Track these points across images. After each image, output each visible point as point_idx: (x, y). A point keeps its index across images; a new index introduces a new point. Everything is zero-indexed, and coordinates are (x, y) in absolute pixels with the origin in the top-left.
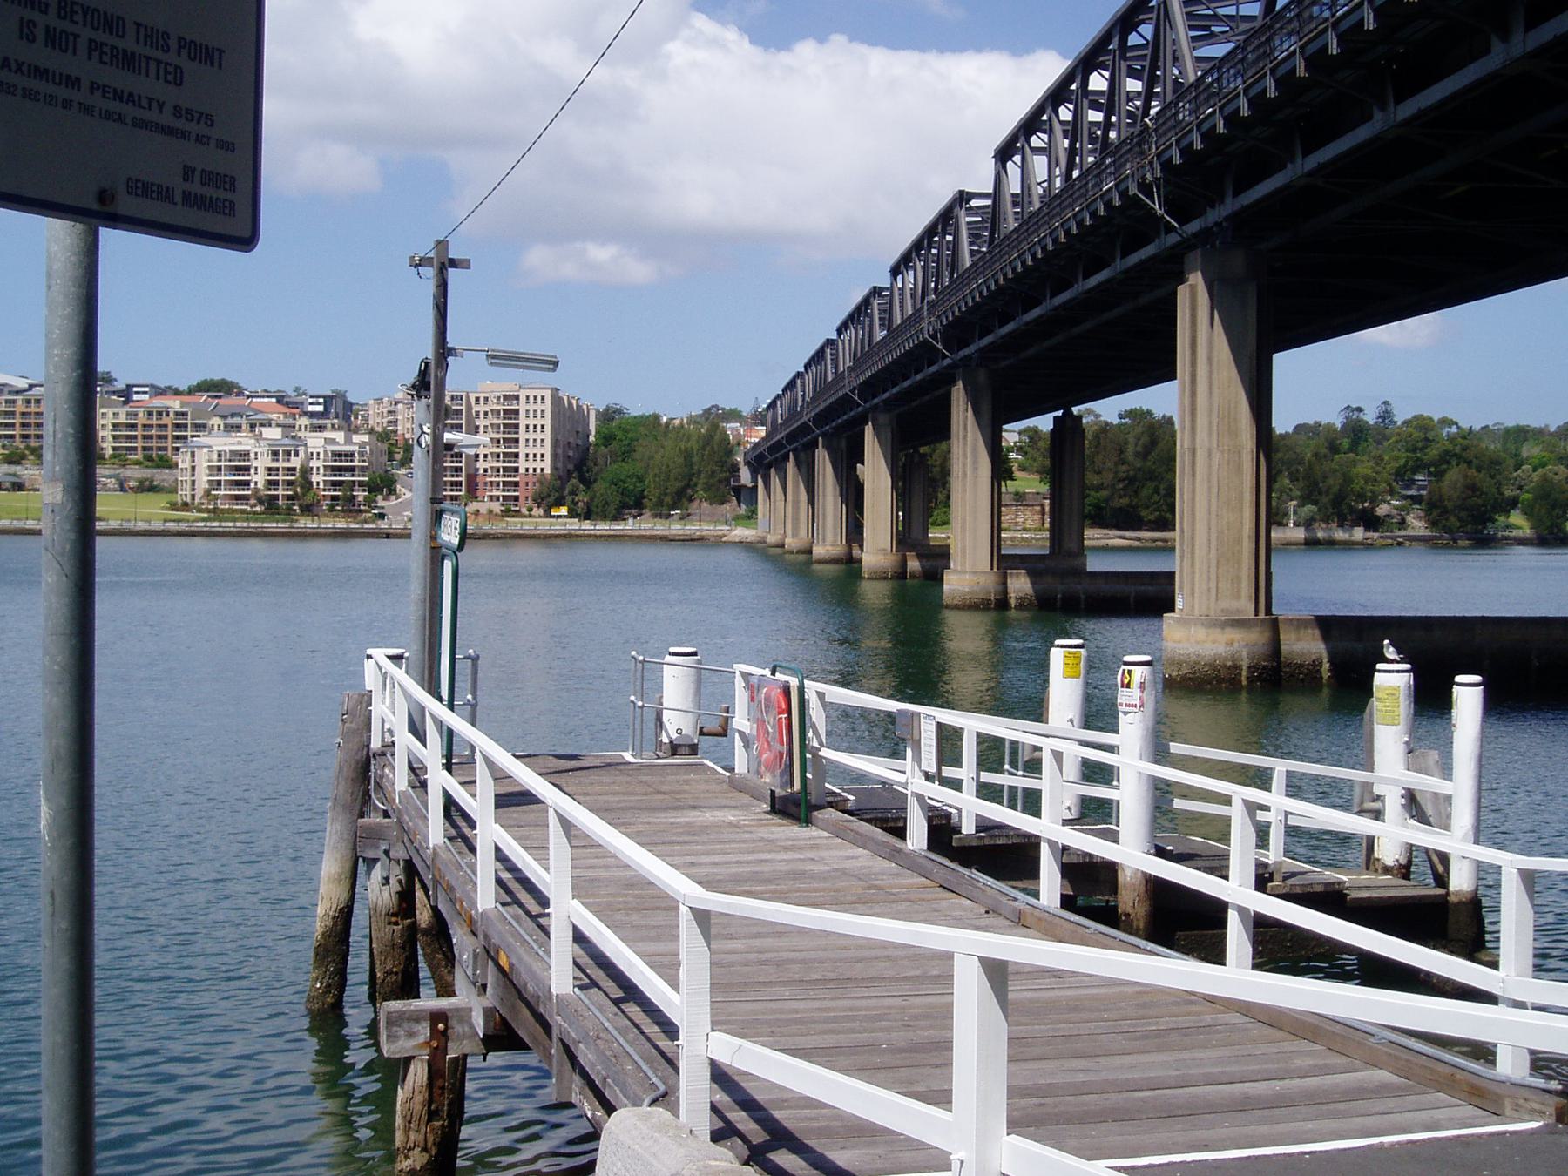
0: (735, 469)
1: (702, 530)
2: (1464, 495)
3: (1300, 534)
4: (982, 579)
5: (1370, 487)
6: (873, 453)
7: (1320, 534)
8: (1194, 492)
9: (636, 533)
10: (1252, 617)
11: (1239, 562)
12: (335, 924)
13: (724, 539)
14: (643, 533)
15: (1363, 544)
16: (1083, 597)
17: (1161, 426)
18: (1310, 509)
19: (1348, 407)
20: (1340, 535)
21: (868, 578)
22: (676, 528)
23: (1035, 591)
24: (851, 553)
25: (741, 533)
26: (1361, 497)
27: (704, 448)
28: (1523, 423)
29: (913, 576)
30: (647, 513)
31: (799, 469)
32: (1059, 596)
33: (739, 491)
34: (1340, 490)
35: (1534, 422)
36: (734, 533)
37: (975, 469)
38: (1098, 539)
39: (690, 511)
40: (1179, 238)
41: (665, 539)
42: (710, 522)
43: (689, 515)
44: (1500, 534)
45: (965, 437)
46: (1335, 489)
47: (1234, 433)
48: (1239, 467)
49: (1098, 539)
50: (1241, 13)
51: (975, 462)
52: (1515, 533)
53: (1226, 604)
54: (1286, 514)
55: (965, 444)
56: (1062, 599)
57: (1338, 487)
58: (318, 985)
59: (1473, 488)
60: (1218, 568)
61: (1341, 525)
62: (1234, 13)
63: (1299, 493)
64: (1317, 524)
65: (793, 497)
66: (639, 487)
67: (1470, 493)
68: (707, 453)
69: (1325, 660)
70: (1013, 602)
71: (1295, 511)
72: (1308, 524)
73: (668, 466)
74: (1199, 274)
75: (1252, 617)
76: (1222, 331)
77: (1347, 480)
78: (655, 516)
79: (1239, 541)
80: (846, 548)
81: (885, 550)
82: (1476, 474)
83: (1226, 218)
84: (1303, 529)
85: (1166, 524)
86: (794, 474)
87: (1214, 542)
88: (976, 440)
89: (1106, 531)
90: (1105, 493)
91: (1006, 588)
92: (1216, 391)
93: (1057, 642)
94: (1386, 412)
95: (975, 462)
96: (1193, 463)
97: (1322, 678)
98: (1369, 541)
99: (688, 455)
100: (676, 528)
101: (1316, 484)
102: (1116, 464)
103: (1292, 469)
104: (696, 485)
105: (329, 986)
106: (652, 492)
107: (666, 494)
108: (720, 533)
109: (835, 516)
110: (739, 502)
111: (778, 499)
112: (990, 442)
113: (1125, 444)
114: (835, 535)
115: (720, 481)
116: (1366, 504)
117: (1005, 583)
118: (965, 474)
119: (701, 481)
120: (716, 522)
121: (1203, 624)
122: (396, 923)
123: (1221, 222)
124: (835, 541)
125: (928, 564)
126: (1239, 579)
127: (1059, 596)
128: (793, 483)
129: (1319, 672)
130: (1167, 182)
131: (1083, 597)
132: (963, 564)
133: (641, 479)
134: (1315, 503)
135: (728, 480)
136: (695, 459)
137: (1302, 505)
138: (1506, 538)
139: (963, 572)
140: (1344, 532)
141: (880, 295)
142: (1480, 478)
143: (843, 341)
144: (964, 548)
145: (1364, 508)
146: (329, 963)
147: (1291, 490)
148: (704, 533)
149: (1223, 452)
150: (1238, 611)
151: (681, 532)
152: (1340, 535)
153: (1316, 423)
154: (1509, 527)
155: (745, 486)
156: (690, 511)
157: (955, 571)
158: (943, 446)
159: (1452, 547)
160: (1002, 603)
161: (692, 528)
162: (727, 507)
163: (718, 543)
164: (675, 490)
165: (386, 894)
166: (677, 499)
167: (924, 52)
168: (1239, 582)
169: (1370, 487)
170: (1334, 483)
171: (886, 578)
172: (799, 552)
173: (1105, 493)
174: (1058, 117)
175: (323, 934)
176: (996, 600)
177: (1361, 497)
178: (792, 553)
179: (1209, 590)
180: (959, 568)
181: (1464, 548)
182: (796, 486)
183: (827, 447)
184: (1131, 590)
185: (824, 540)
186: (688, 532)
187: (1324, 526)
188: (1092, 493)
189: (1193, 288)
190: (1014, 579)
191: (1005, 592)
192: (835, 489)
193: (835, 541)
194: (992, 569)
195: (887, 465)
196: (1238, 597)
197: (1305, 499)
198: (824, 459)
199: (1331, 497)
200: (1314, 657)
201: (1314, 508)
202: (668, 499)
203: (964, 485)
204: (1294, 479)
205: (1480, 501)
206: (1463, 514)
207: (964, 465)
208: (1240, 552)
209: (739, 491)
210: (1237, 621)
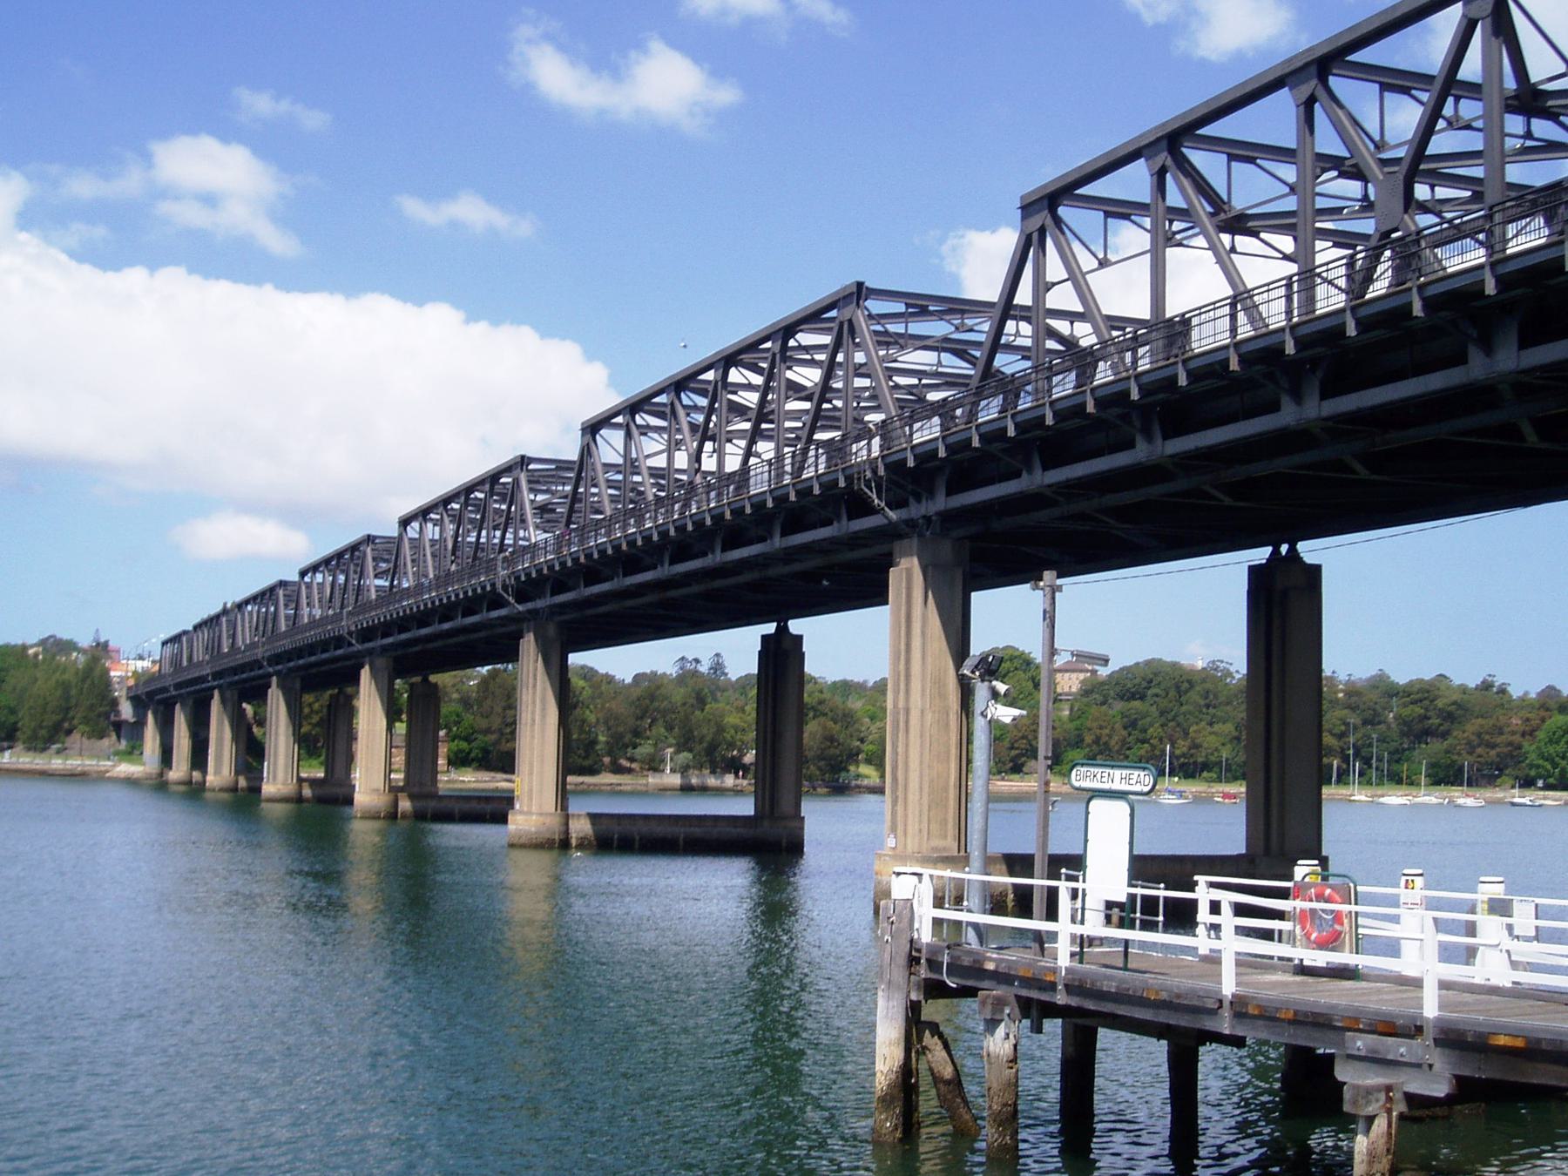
0: (114, 703)
1: (84, 765)
2: (823, 746)
3: (676, 780)
4: (548, 820)
5: (739, 736)
6: (370, 696)
7: (694, 781)
8: (907, 745)
9: (14, 767)
10: (956, 854)
11: (946, 807)
12: (897, 1077)
13: (108, 775)
14: (20, 766)
15: (734, 791)
16: (637, 838)
17: (176, 661)
18: (685, 756)
19: (683, 658)
20: (712, 781)
21: (361, 818)
22: (57, 763)
23: (594, 831)
24: (301, 793)
25: (125, 769)
26: (731, 746)
27: (84, 680)
28: (849, 678)
29: (404, 816)
30: (20, 747)
31: (225, 708)
32: (616, 836)
33: (118, 726)
34: (713, 739)
35: (856, 676)
36: (118, 769)
37: (544, 716)
38: (485, 781)
39: (66, 745)
40: (886, 521)
41: (44, 774)
42: (92, 757)
43: (66, 749)
44: (853, 783)
45: (535, 686)
46: (708, 738)
47: (943, 696)
48: (947, 725)
49: (485, 781)
50: (909, 332)
51: (544, 709)
52: (866, 782)
53: (937, 843)
54: (663, 761)
55: (534, 693)
56: (618, 838)
57: (711, 736)
58: (888, 1124)
59: (831, 739)
60: (929, 811)
61: (713, 772)
62: (903, 331)
63: (674, 742)
64: (691, 771)
65: (217, 733)
66: (12, 719)
67: (829, 744)
68: (86, 686)
69: (1010, 892)
70: (574, 842)
71: (671, 759)
72: (684, 770)
73: (45, 699)
74: (915, 560)
75: (956, 854)
76: (934, 605)
77: (721, 729)
78: (29, 749)
79: (946, 789)
80: (296, 787)
81: (378, 790)
82: (833, 726)
83: (938, 514)
84: (679, 775)
85: (513, 772)
86: (219, 712)
87: (926, 789)
88: (544, 689)
89: (492, 774)
90: (493, 737)
91: (568, 829)
92: (929, 660)
93: (1300, 862)
94: (718, 663)
95: (544, 709)
96: (907, 722)
97: (1007, 907)
98: (739, 788)
99: (65, 687)
100: (57, 763)
101: (691, 731)
102: (504, 709)
103: (668, 718)
104: (73, 718)
105: (896, 1125)
106: (26, 723)
107: (41, 727)
108: (103, 769)
109: (287, 756)
110: (119, 738)
111: (182, 734)
112: (558, 691)
113: (1460, 723)
114: (286, 772)
115: (99, 715)
116: (735, 753)
117: (567, 824)
118: (533, 720)
119: (79, 715)
120: (99, 758)
121: (917, 861)
122: (1012, 1068)
123: (930, 517)
124: (287, 780)
125: (421, 804)
126: (945, 820)
127: (616, 836)
128: (218, 720)
129: (1005, 902)
130: (889, 481)
131: (637, 838)
132: (530, 805)
133: (13, 711)
134: (690, 750)
135: (108, 717)
136: (73, 692)
137: (677, 752)
138: (858, 787)
139: (529, 813)
140: (716, 778)
141: (373, 543)
142: (835, 728)
143: (309, 586)
144: (531, 790)
145: (733, 757)
146: (895, 1107)
147: (666, 737)
148: (86, 769)
149: (934, 712)
150: (945, 849)
151: (61, 767)
152: (712, 781)
153: (652, 672)
154: (858, 776)
155: (126, 722)
156: (66, 745)
157: (521, 812)
158: (349, 690)
159: (812, 794)
160: (565, 844)
161: (74, 763)
162: (106, 742)
163: (101, 778)
164: (50, 724)
165: (1006, 1046)
166: (50, 735)
167: (288, 292)
168: (946, 824)
169: (739, 736)
170: (707, 732)
171: (379, 818)
172: (222, 790)
173: (493, 737)
174: (681, 402)
175: (889, 1085)
176: (561, 840)
177: (731, 746)
178: (214, 790)
179: (920, 830)
180: (525, 809)
181: (821, 795)
182: (220, 724)
183: (281, 686)
184: (680, 831)
185: (275, 778)
186: (69, 767)
187: (696, 772)
188: (480, 737)
189: (909, 572)
190: (575, 821)
191: (567, 832)
192: (287, 728)
193: (287, 780)
194: (556, 809)
195: (383, 705)
196: (945, 837)
197: (680, 748)
198: (278, 700)
199: (705, 745)
200: (1001, 889)
201: (690, 756)
202: (43, 732)
203: (532, 731)
204: (670, 728)
205: (838, 752)
206: (822, 763)
207: (533, 713)
208: (947, 798)
209: (118, 726)
210: (947, 857)
